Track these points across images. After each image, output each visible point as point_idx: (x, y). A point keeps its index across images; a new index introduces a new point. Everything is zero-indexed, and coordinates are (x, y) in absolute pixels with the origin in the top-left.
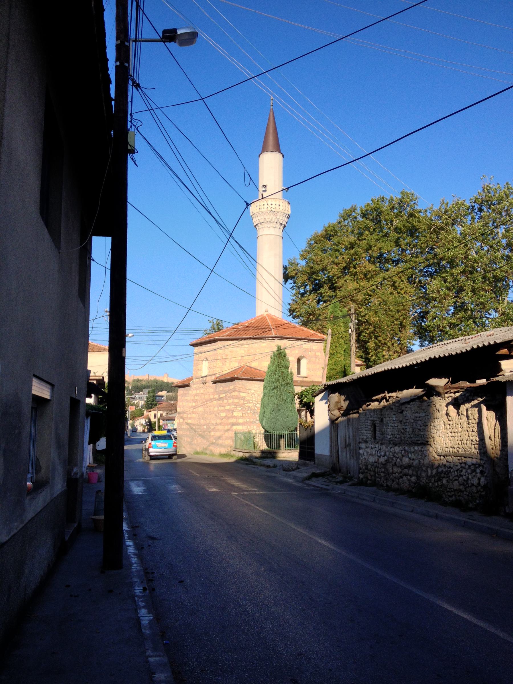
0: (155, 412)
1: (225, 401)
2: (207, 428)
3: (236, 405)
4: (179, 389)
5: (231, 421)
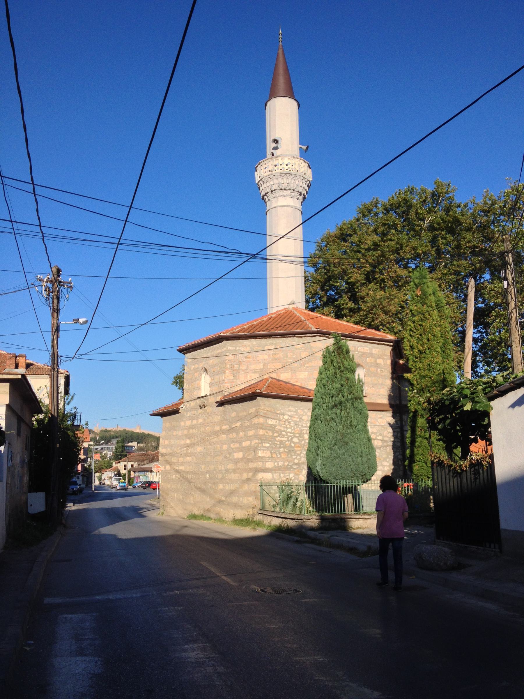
0: (126, 463)
1: (242, 434)
2: (210, 478)
3: (262, 439)
5: (251, 465)
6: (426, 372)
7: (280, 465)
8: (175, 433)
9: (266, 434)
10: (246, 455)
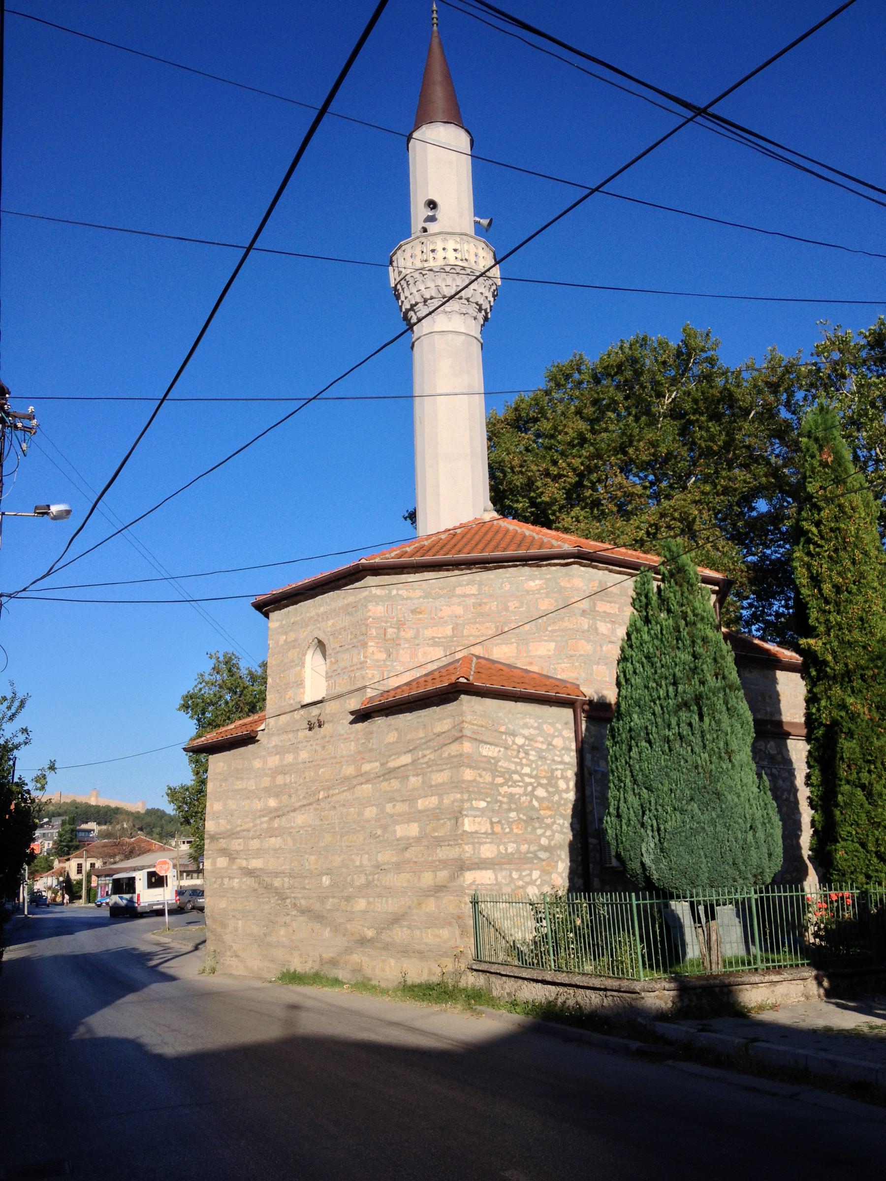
0: (81, 861)
3: (471, 790)
4: (212, 758)
5: (443, 853)
6: (856, 635)
7: (509, 851)
8: (239, 785)
9: (478, 779)
10: (429, 828)
